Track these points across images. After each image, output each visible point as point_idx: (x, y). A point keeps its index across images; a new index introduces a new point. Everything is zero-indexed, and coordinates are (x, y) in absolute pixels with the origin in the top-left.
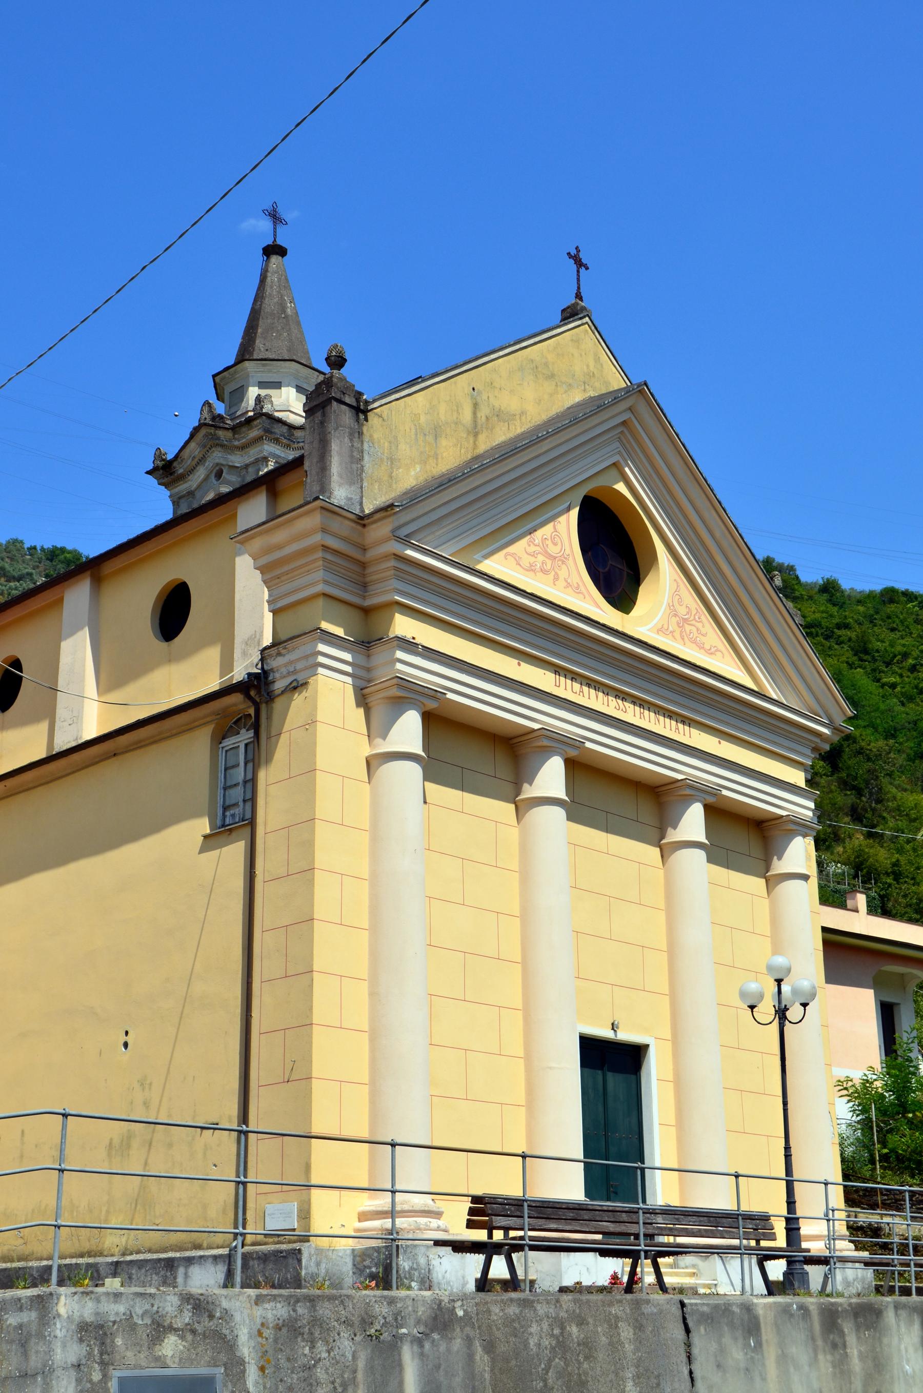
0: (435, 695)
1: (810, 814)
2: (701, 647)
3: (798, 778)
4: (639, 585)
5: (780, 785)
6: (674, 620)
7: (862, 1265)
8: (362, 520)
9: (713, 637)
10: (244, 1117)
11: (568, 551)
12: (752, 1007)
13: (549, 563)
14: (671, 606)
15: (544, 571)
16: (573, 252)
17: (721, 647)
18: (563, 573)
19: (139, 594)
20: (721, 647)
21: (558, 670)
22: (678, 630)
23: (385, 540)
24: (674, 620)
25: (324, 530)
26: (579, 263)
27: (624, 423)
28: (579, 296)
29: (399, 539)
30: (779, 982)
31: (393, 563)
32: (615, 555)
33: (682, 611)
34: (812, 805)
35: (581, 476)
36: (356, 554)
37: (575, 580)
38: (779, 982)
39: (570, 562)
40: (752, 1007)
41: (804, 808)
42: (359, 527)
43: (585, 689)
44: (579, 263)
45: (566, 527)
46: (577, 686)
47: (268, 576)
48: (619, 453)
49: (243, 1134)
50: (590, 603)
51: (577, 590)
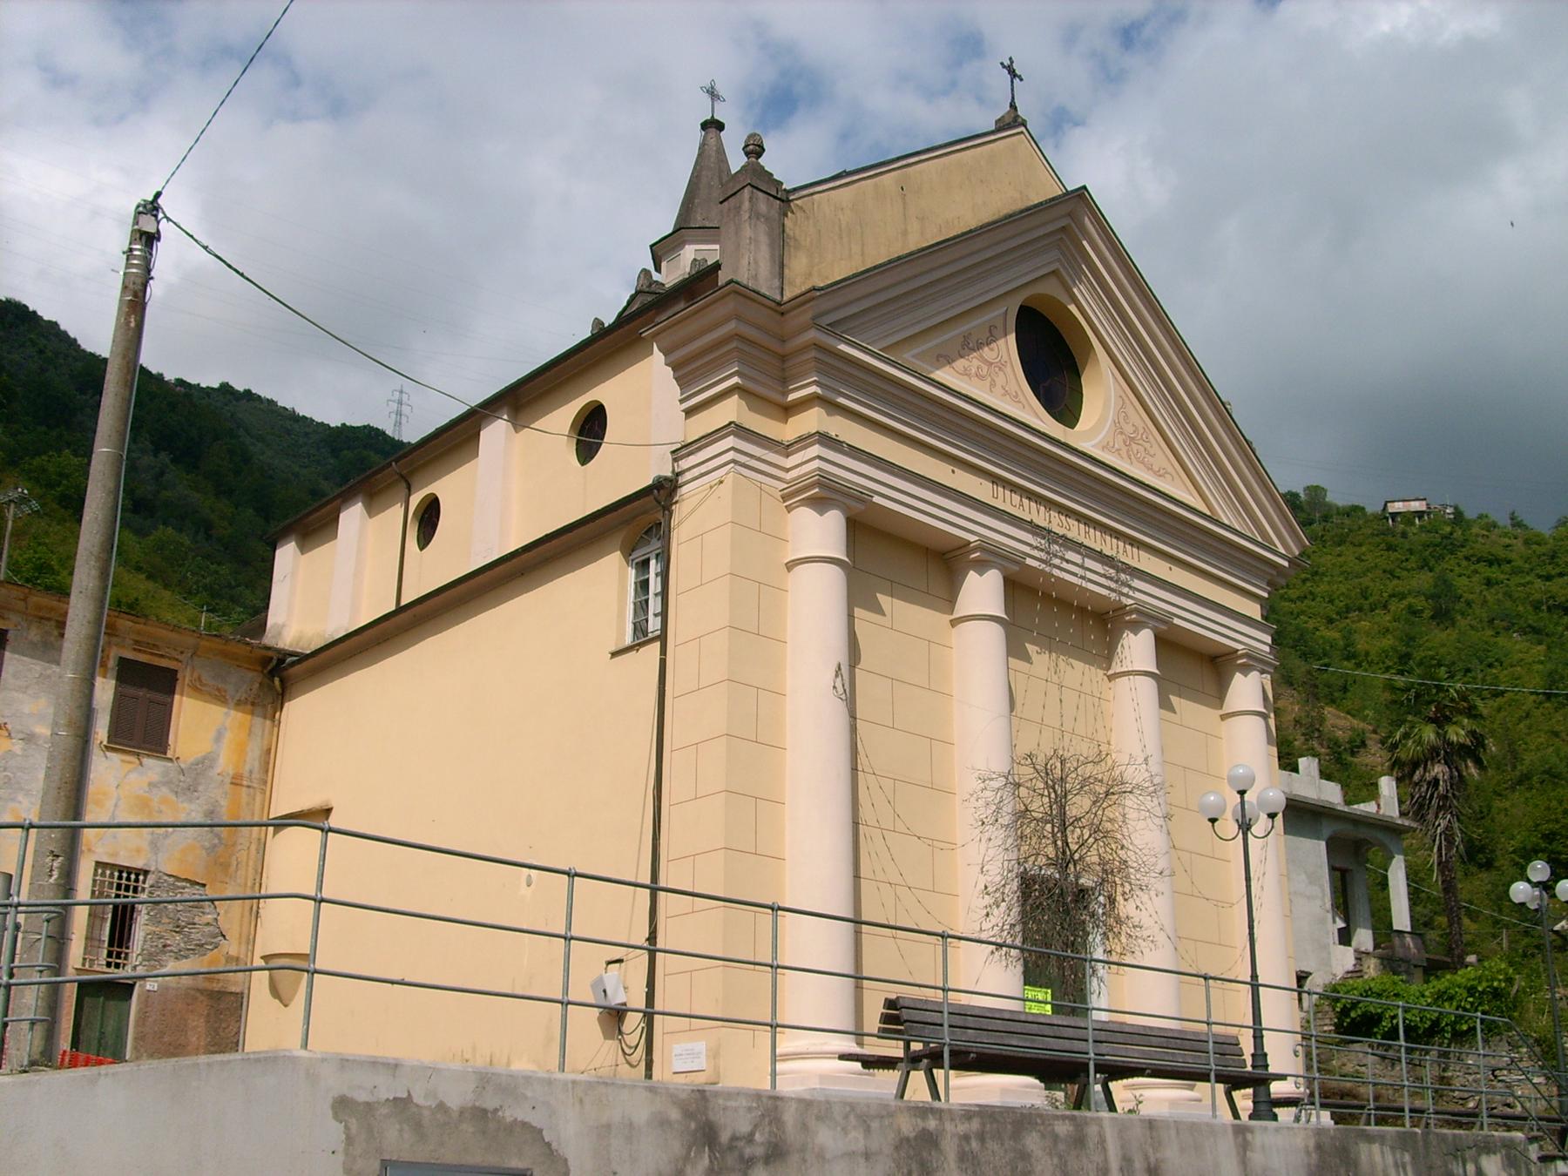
0: (862, 497)
1: (1267, 649)
2: (1150, 468)
3: (1254, 610)
4: (1077, 375)
5: (1232, 616)
6: (1120, 438)
7: (858, 1065)
8: (780, 309)
9: (1162, 458)
10: (652, 938)
11: (1005, 358)
12: (1213, 821)
13: (985, 368)
14: (1116, 423)
15: (982, 378)
16: (1007, 63)
17: (1170, 469)
18: (1000, 380)
19: (563, 417)
20: (1170, 469)
21: (996, 480)
22: (1124, 449)
23: (805, 329)
24: (1120, 438)
25: (738, 318)
26: (1013, 73)
27: (1063, 229)
28: (1013, 106)
29: (819, 327)
30: (1242, 793)
31: (813, 354)
32: (1053, 362)
33: (1129, 429)
34: (1268, 639)
35: (1019, 280)
36: (774, 345)
37: (1013, 387)
38: (1242, 793)
39: (1008, 370)
40: (1213, 821)
41: (1261, 641)
42: (778, 317)
43: (1026, 501)
44: (1013, 73)
45: (1007, 347)
46: (1016, 498)
47: (681, 373)
48: (1059, 260)
49: (652, 954)
50: (1031, 411)
51: (1015, 398)
